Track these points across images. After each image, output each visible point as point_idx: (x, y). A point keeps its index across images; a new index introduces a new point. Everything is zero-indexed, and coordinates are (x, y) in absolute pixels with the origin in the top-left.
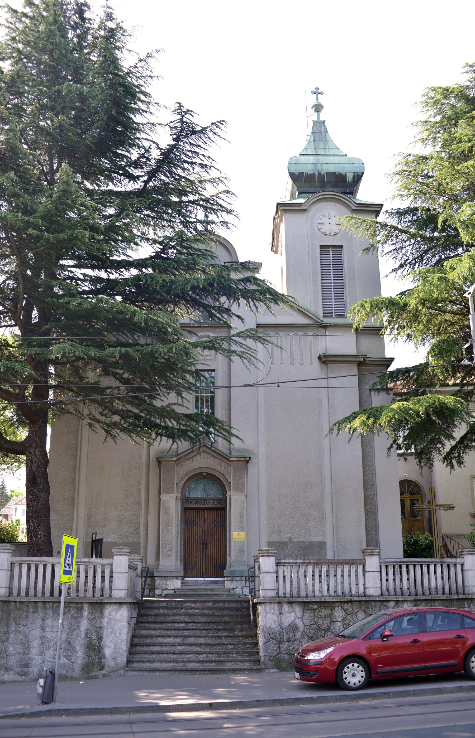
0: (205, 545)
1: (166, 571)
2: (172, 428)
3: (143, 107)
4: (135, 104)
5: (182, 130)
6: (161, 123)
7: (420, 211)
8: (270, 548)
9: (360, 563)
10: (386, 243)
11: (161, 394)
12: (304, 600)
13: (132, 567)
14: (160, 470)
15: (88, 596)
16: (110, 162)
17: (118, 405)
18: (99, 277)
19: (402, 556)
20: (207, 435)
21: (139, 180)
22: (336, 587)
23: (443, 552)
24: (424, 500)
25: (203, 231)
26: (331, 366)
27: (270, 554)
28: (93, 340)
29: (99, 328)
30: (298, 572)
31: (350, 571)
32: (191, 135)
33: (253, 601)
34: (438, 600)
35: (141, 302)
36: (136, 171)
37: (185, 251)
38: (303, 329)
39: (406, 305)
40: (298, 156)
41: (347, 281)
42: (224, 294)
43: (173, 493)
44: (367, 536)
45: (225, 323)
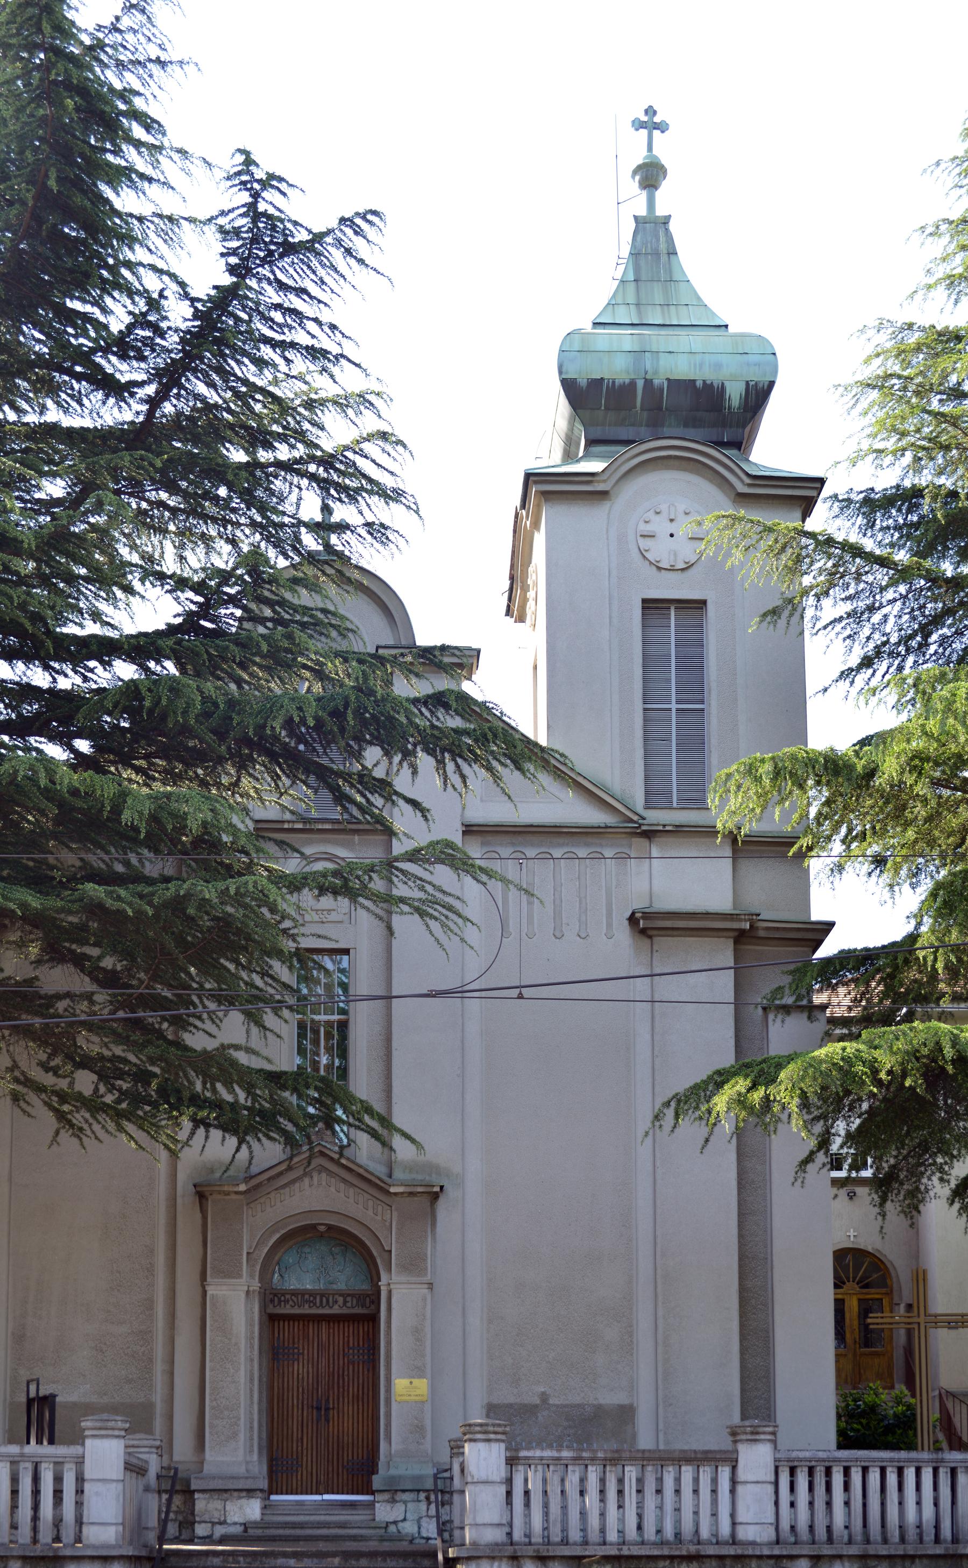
0: (322, 1410)
1: (221, 1478)
2: (234, 1106)
3: (141, 165)
4: (117, 152)
5: (255, 240)
6: (194, 215)
7: (927, 500)
8: (490, 1421)
9: (724, 1460)
10: (827, 593)
11: (205, 1016)
12: (578, 1551)
13: (134, 1468)
14: (205, 1218)
15: (21, 1541)
16: (47, 335)
17: (90, 1044)
18: (28, 685)
19: (833, 1443)
20: (329, 1126)
21: (132, 395)
22: (660, 1519)
23: (941, 1436)
24: (896, 1300)
25: (318, 552)
26: (662, 942)
27: (492, 1436)
28: (17, 862)
29: (33, 831)
30: (563, 1480)
31: (696, 1480)
32: (282, 256)
33: (445, 1552)
34: (921, 1557)
35: (147, 757)
36: (124, 367)
37: (268, 612)
38: (590, 840)
39: (871, 773)
40: (588, 327)
41: (714, 703)
42: (377, 740)
43: (240, 1276)
44: (743, 1390)
45: (380, 820)
